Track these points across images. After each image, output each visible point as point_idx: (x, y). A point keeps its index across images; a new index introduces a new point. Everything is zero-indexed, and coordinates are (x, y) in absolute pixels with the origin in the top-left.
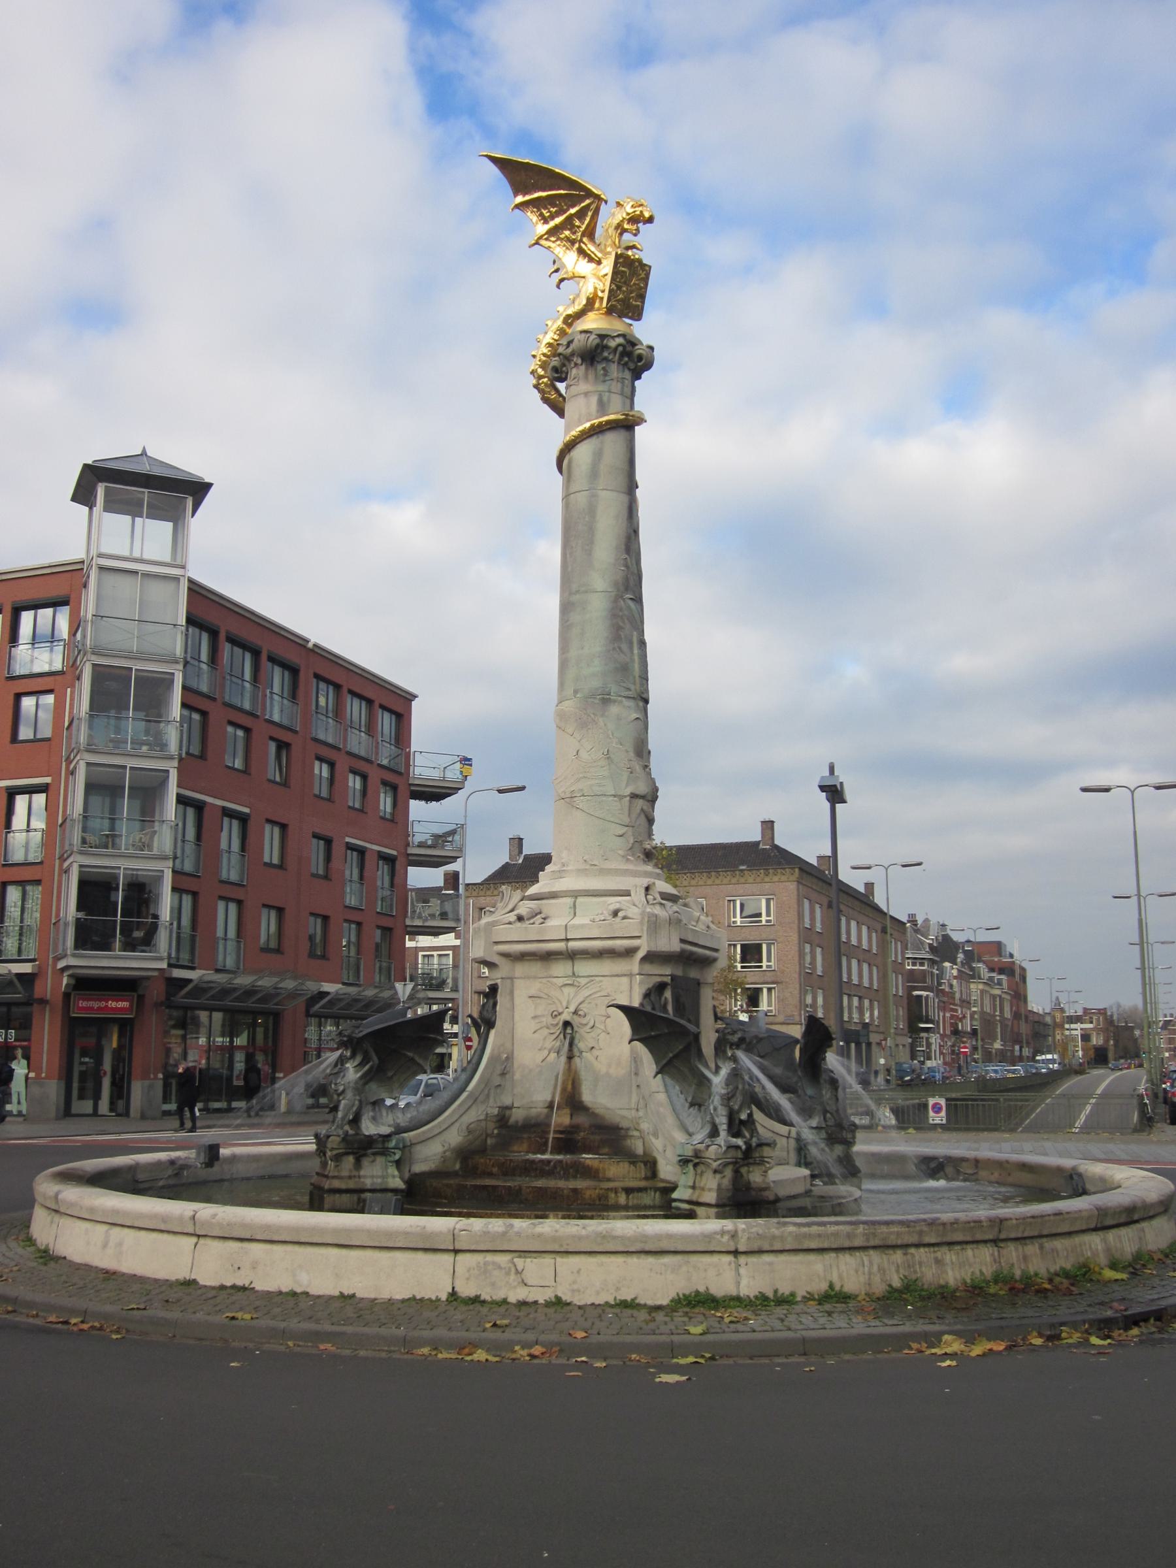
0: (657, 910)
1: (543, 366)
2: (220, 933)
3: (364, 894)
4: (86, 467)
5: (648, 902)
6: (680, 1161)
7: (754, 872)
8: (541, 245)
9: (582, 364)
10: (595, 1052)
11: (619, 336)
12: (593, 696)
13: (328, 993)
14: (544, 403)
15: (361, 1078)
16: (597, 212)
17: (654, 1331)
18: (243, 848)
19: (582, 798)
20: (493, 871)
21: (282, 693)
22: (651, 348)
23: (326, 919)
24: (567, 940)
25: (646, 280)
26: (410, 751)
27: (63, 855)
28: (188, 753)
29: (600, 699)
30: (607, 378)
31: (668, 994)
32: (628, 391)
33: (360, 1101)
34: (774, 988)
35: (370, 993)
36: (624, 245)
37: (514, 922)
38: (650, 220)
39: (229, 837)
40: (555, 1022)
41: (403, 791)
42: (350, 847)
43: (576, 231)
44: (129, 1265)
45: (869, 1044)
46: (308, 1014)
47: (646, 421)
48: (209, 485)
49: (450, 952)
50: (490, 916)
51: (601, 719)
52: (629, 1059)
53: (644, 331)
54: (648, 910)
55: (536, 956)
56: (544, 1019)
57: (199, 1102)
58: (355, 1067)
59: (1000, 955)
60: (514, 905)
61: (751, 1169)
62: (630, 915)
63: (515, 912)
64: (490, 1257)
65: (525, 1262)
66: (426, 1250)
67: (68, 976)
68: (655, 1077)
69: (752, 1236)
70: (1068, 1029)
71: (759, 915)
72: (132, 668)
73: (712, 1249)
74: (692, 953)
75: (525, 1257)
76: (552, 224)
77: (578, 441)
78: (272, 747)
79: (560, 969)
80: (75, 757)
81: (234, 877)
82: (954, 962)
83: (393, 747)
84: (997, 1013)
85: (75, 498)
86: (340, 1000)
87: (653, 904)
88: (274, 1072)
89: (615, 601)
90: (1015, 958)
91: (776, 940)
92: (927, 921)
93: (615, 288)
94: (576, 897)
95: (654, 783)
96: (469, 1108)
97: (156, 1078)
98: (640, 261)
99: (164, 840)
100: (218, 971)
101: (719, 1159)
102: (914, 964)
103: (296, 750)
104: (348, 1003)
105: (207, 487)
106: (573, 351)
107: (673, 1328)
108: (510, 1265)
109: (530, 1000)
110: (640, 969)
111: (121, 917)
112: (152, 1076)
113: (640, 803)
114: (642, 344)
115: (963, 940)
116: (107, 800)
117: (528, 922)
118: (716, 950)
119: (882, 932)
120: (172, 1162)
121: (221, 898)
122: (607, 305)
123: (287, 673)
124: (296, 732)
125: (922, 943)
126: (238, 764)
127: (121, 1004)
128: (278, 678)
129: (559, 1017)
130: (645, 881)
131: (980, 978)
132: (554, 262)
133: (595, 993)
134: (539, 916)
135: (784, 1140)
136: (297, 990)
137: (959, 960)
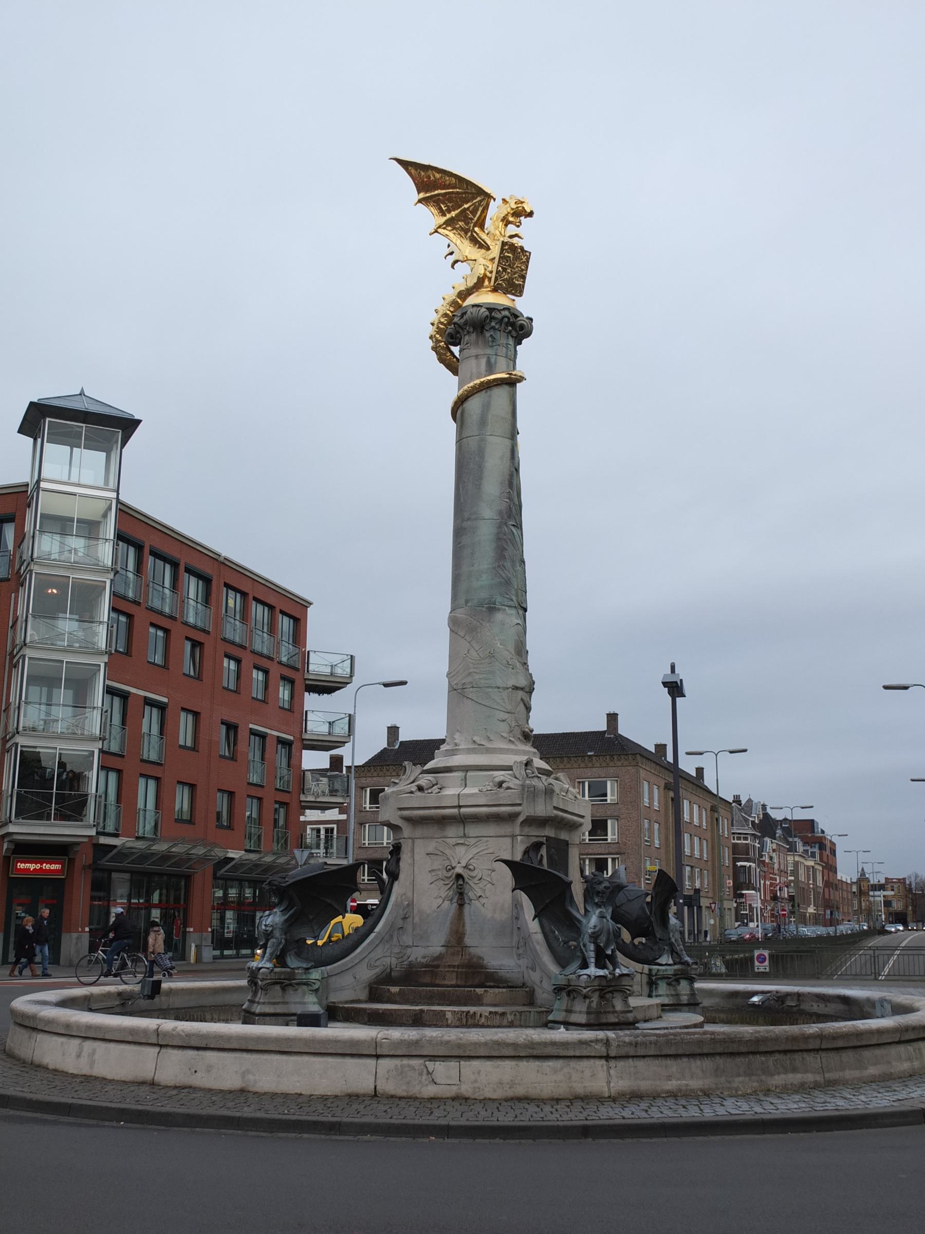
0: (535, 782)
1: (439, 331)
2: (140, 805)
3: (265, 772)
4: (32, 404)
5: (527, 776)
6: (555, 989)
7: (601, 757)
8: (440, 233)
9: (473, 332)
10: (483, 900)
11: (504, 309)
12: (481, 605)
13: (233, 859)
14: (440, 362)
15: (286, 921)
16: (486, 207)
17: (542, 1118)
18: (162, 732)
19: (471, 689)
20: (373, 755)
21: (197, 599)
22: (531, 319)
23: (231, 794)
24: (460, 807)
25: (527, 263)
26: (305, 650)
27: (6, 736)
28: (116, 651)
29: (487, 608)
30: (494, 344)
31: (544, 851)
32: (511, 353)
33: (286, 940)
34: (618, 858)
35: (269, 859)
36: (508, 235)
37: (416, 791)
38: (531, 214)
39: (150, 722)
40: (449, 875)
41: (299, 685)
42: (253, 733)
43: (469, 222)
44: (101, 1070)
45: (700, 907)
46: (215, 877)
47: (525, 379)
48: (138, 422)
49: (335, 826)
50: (393, 787)
51: (488, 625)
52: (511, 906)
53: (523, 305)
54: (528, 782)
55: (434, 820)
56: (439, 873)
57: (229, 909)
58: (281, 911)
59: (813, 831)
60: (415, 777)
61: (614, 996)
62: (512, 786)
63: (416, 783)
64: (405, 1061)
65: (435, 1064)
66: (352, 1055)
67: (9, 841)
68: (533, 920)
69: (621, 1044)
70: (872, 896)
71: (605, 795)
72: (69, 577)
73: (588, 1054)
74: (563, 819)
75: (435, 1061)
76: (448, 216)
77: (469, 395)
78: (188, 646)
79: (453, 831)
80: (17, 653)
81: (153, 757)
82: (773, 837)
83: (291, 646)
84: (811, 882)
85: (22, 430)
86: (242, 865)
87: (532, 777)
88: (185, 926)
89: (499, 527)
90: (825, 833)
91: (619, 817)
92: (750, 801)
93: (501, 270)
94: (467, 771)
95: (532, 677)
96: (377, 945)
97: (83, 931)
98: (522, 248)
99: (94, 722)
100: (138, 838)
101: (588, 987)
102: (739, 839)
103: (208, 649)
104: (249, 868)
105: (136, 423)
106: (466, 321)
107: (558, 1116)
108: (422, 1067)
109: (427, 856)
110: (522, 831)
111: (56, 790)
112: (80, 929)
113: (520, 694)
114: (523, 316)
115: (781, 819)
116: (45, 689)
117: (426, 792)
118: (582, 817)
119: (711, 810)
120: (120, 994)
121: (142, 775)
122: (494, 283)
123: (201, 582)
124: (208, 633)
125: (746, 820)
126: (159, 659)
127: (54, 867)
128: (193, 587)
129: (452, 871)
130: (524, 758)
131: (796, 851)
132: (449, 246)
133: (483, 850)
134: (435, 787)
135: (639, 975)
136: (206, 856)
137: (777, 835)
